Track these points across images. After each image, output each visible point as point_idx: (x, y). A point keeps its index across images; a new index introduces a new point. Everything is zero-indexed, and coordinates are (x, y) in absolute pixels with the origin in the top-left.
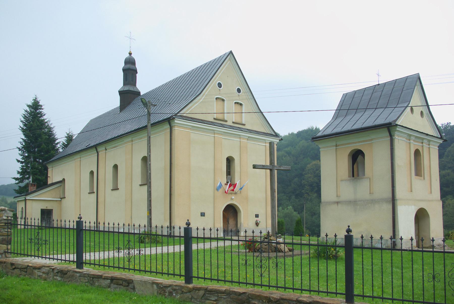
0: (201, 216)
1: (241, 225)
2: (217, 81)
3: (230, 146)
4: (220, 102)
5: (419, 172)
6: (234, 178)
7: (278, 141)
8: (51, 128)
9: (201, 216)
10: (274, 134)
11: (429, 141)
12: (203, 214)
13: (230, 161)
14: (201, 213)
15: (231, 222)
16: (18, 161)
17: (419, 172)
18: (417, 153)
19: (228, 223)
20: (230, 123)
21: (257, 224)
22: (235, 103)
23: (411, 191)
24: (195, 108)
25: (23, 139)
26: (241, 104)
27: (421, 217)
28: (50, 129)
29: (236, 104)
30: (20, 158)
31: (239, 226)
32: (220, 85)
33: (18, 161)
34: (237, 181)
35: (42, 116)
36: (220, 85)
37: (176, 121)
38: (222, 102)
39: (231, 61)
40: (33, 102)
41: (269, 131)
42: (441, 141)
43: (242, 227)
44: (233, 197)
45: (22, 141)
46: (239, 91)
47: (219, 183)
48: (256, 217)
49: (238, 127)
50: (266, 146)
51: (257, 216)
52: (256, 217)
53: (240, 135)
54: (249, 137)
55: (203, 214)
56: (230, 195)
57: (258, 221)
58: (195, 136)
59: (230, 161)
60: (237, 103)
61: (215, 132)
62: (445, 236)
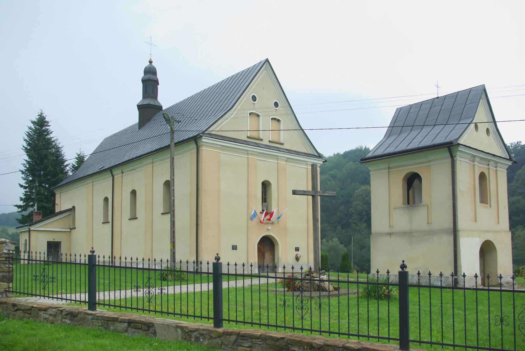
0: (233, 249)
1: (278, 260)
2: (250, 94)
3: (266, 168)
4: (255, 118)
5: (484, 198)
6: (271, 206)
7: (321, 163)
8: (59, 148)
9: (233, 249)
10: (316, 154)
11: (496, 163)
12: (234, 248)
13: (266, 186)
14: (233, 246)
15: (268, 256)
16: (21, 186)
17: (484, 198)
18: (482, 176)
19: (264, 258)
20: (266, 142)
21: (297, 259)
22: (272, 119)
23: (476, 221)
24: (225, 124)
25: (26, 161)
26: (279, 121)
27: (487, 250)
28: (58, 149)
29: (273, 120)
30: (23, 182)
31: (276, 261)
32: (254, 98)
33: (21, 186)
34: (274, 209)
35: (48, 134)
36: (254, 98)
37: (203, 140)
38: (256, 118)
39: (267, 71)
40: (38, 117)
41: (311, 151)
42: (510, 163)
43: (279, 263)
44: (270, 228)
45: (25, 162)
46: (276, 105)
47: (253, 211)
48: (296, 251)
49: (275, 147)
50: (307, 168)
51: (297, 249)
52: (296, 251)
53: (277, 156)
54: (288, 158)
55: (234, 248)
56: (266, 225)
57: (299, 256)
58: (226, 157)
59: (266, 186)
60: (275, 119)
61: (249, 152)
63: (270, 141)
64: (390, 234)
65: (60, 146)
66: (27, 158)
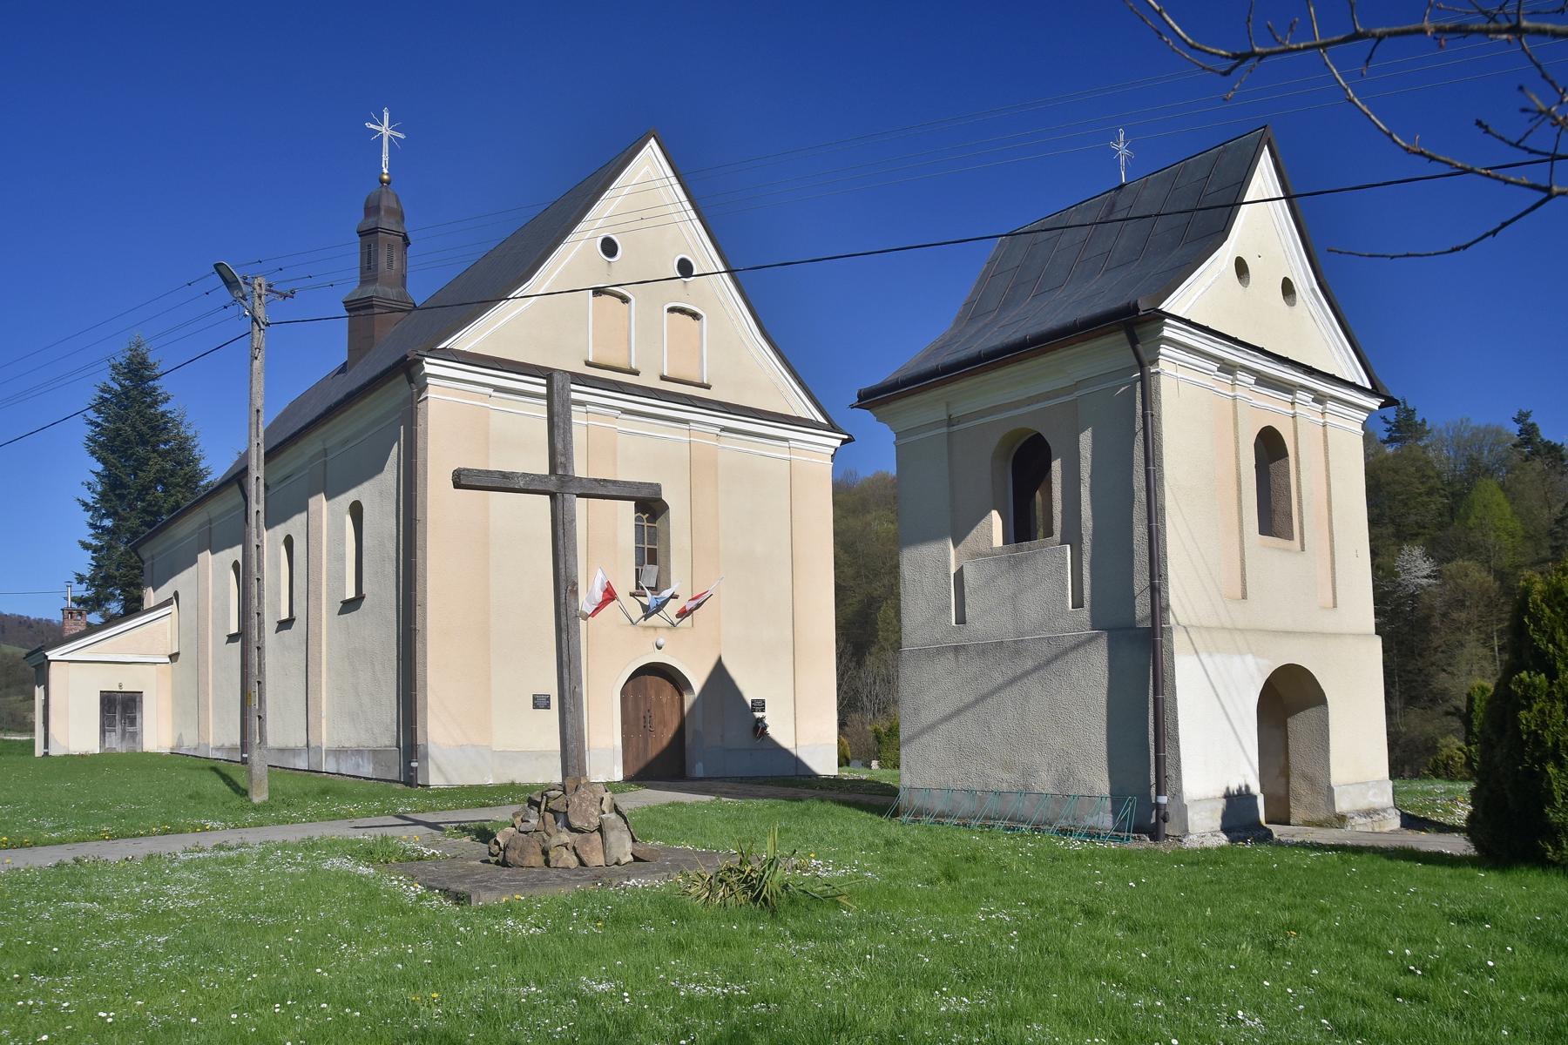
0: (536, 706)
5: (1274, 514)
7: (837, 443)
8: (187, 439)
9: (536, 706)
11: (1320, 399)
14: (535, 698)
16: (86, 546)
17: (1274, 514)
18: (1270, 446)
23: (1244, 597)
25: (97, 474)
27: (1289, 699)
28: (184, 446)
30: (87, 534)
32: (609, 247)
33: (86, 546)
35: (155, 403)
36: (609, 247)
40: (128, 354)
42: (1374, 403)
45: (93, 478)
54: (724, 429)
62: (158, 427)
63: (588, 364)
64: (957, 649)
65: (190, 433)
66: (99, 467)
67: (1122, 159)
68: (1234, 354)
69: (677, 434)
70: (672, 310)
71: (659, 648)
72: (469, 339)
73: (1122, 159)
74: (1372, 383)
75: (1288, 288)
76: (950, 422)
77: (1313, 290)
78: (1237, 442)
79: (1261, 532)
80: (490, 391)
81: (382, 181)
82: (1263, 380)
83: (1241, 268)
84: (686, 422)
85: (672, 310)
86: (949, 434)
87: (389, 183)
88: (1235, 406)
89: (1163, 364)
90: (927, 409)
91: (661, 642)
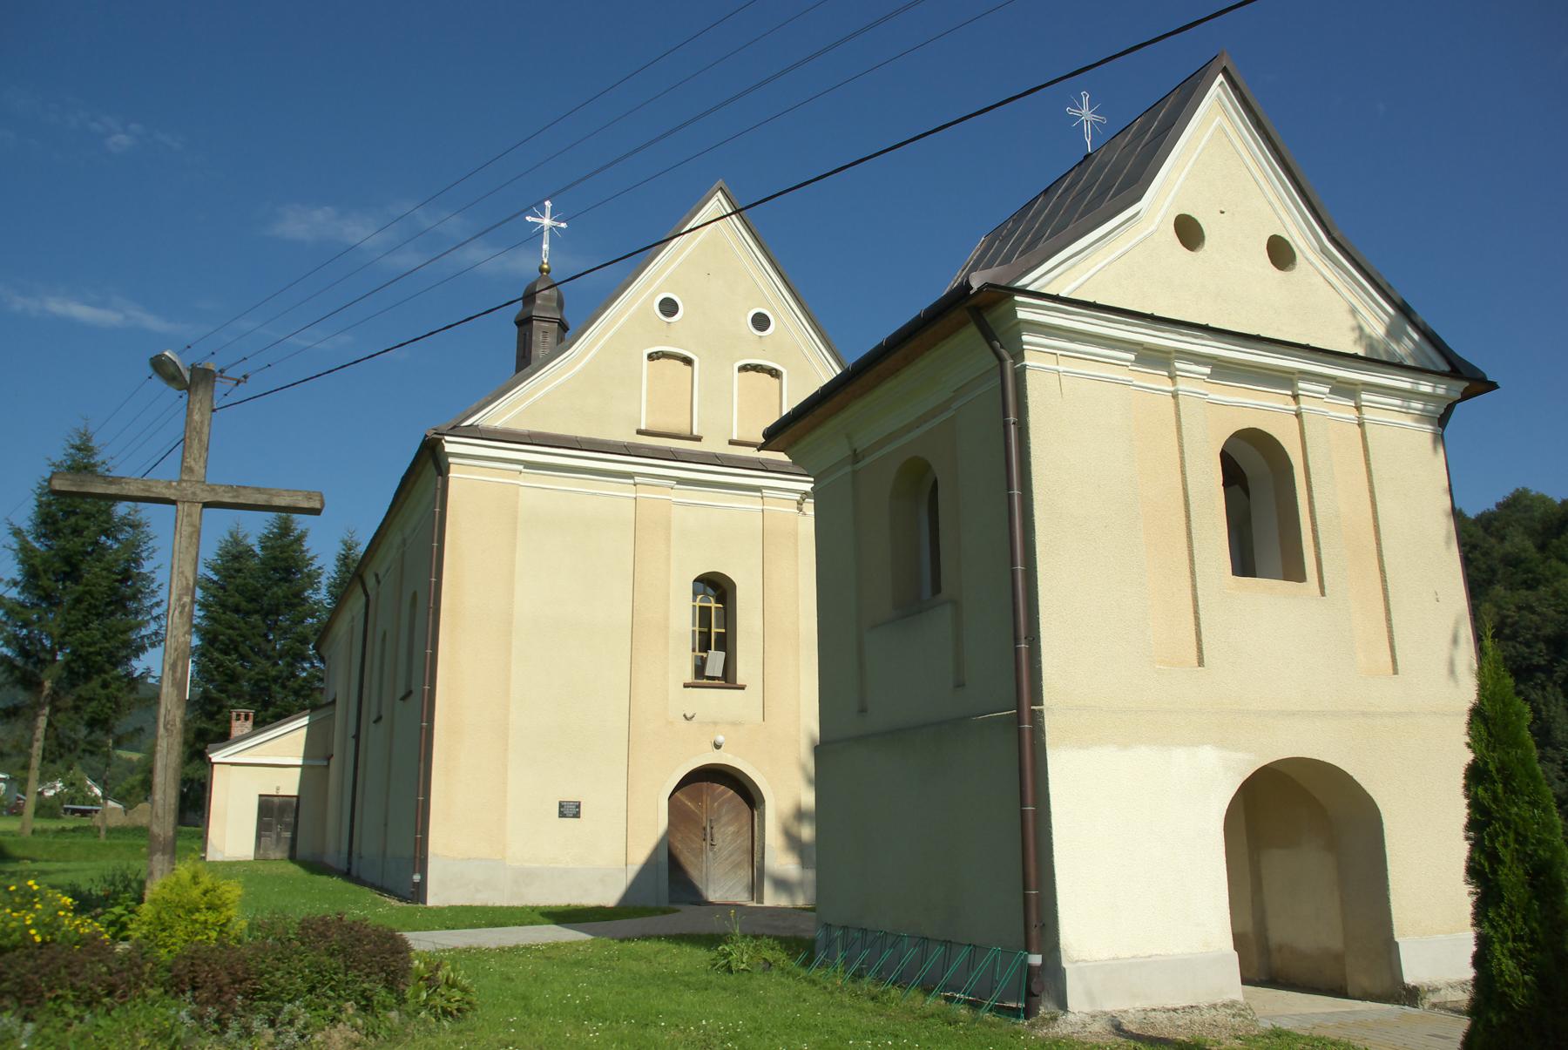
0: (562, 815)
2: (653, 296)
9: (562, 815)
12: (570, 810)
14: (561, 805)
27: (1295, 824)
32: (669, 307)
46: (761, 322)
55: (570, 810)
67: (1087, 128)
68: (1154, 339)
69: (750, 503)
70: (744, 368)
71: (718, 746)
72: (498, 415)
73: (1087, 128)
74: (1450, 363)
75: (1281, 254)
76: (856, 457)
77: (1324, 251)
78: (1182, 452)
79: (1235, 573)
80: (520, 467)
81: (541, 270)
82: (1223, 370)
83: (1189, 232)
84: (630, 475)
85: (744, 368)
86: (855, 473)
87: (548, 272)
88: (1177, 405)
89: (1031, 359)
90: (831, 441)
91: (720, 739)
